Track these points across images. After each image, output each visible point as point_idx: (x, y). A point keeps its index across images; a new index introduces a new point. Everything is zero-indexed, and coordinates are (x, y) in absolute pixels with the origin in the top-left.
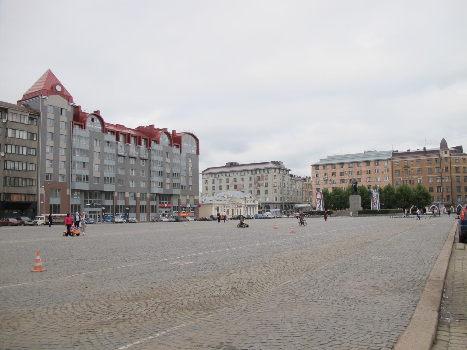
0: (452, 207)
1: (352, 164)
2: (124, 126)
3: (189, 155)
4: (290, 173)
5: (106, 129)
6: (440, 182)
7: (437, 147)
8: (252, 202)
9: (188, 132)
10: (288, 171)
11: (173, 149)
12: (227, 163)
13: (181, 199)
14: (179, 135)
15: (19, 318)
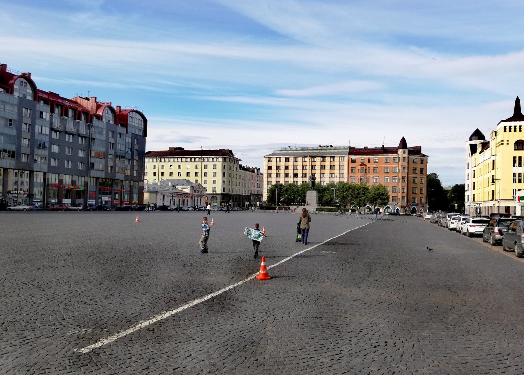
0: (407, 208)
2: (59, 95)
3: (134, 136)
4: (240, 163)
5: (39, 96)
6: (395, 182)
8: (200, 192)
9: (135, 109)
10: (238, 160)
11: (118, 128)
12: (170, 148)
13: (124, 185)
14: (124, 113)
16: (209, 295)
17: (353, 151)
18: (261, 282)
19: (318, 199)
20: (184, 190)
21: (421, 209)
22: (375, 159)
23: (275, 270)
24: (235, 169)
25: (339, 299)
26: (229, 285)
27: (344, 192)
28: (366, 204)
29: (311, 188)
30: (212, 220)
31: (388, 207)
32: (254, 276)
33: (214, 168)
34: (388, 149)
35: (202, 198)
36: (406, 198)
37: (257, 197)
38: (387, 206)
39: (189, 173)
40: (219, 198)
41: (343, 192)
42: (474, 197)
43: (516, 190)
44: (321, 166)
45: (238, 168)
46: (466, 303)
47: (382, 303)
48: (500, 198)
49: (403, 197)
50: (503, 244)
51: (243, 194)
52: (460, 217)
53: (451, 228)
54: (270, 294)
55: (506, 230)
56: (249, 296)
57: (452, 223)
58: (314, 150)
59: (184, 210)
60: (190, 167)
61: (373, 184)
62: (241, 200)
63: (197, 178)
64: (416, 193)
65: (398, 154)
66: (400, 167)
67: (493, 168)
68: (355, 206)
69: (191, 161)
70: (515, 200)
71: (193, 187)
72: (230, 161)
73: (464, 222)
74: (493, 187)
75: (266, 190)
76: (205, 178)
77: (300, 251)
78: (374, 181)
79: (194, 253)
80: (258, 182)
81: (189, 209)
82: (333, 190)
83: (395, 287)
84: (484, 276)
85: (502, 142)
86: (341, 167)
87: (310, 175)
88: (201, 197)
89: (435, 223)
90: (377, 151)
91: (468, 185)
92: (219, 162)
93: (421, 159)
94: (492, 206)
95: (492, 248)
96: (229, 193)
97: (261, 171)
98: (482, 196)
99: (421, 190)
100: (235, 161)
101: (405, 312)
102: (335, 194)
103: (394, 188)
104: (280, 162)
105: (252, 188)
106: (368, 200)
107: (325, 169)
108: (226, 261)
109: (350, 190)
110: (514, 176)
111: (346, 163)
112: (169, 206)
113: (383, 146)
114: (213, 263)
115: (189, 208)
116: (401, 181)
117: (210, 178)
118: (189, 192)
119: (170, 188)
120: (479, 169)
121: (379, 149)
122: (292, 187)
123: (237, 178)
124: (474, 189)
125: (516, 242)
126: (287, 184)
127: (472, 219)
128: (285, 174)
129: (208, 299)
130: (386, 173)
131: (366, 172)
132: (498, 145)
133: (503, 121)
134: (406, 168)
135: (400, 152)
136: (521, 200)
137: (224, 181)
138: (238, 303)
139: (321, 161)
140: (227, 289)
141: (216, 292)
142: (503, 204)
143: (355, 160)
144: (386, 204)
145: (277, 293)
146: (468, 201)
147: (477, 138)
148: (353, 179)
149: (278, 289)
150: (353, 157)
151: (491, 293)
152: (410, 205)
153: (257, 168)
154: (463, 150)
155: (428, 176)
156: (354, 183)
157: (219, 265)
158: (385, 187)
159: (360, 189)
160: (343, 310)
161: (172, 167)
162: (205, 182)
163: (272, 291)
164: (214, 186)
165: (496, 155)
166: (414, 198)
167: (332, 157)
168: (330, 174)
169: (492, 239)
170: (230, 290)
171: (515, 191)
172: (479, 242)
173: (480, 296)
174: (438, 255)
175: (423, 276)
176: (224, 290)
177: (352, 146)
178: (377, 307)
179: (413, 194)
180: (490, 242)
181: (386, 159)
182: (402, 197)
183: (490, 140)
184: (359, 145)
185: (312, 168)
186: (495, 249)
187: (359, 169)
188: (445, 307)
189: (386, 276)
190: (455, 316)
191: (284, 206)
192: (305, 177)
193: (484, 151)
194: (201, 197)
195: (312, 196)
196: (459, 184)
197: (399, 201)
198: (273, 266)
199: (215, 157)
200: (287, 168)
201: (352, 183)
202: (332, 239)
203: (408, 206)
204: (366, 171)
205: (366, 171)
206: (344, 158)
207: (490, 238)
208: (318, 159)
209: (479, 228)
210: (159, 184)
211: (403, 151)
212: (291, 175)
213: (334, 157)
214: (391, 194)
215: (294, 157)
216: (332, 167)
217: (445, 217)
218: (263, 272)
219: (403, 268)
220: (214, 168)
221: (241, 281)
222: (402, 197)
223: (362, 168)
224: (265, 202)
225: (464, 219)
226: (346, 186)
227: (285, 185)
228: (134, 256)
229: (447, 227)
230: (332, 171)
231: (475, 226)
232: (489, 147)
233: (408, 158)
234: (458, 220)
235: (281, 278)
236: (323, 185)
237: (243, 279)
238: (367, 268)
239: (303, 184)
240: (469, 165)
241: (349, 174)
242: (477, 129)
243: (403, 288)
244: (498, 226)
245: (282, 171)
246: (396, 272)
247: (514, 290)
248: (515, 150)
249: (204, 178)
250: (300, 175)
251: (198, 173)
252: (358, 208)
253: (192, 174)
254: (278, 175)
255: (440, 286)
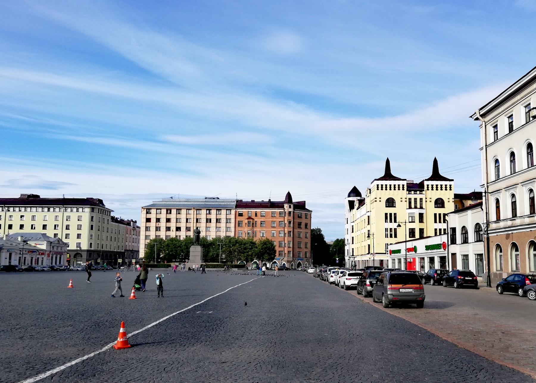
0: (292, 262)
1: (191, 210)
4: (112, 214)
6: (282, 237)
7: (282, 199)
8: (59, 248)
10: (110, 211)
12: (22, 195)
13: (115, 241)
15: (453, 319)
16: (48, 372)
17: (240, 204)
18: (118, 351)
19: (202, 255)
20: (38, 246)
21: (306, 264)
22: (262, 212)
23: (139, 336)
24: (106, 221)
25: (205, 363)
26: (77, 358)
27: (231, 247)
28: (254, 260)
29: (195, 242)
30: (71, 282)
31: (275, 262)
32: (111, 344)
33: (78, 220)
34: (275, 203)
35: (62, 256)
36: (292, 252)
37: (132, 253)
38: (274, 261)
39: (46, 225)
40: (85, 255)
41: (230, 247)
42: (353, 251)
43: (388, 244)
44: (207, 219)
45: (110, 220)
46: (332, 355)
47: (250, 362)
48: (375, 252)
49: (289, 252)
50: (373, 295)
51: (116, 251)
52: (339, 270)
53: (331, 281)
54: (126, 365)
55: (375, 282)
56: (100, 369)
57: (332, 276)
58: (196, 202)
59: (38, 271)
60: (47, 218)
61: (260, 238)
62: (113, 257)
63: (56, 232)
64: (301, 248)
65: (284, 209)
66: (286, 222)
67: (369, 224)
68: (242, 262)
69: (49, 210)
70: (388, 254)
71: (51, 243)
72: (100, 212)
73: (342, 275)
74: (369, 242)
75: (144, 245)
76: (68, 232)
77: (172, 313)
78: (261, 236)
79: (38, 322)
80: (134, 236)
81: (45, 269)
82: (219, 245)
83: (267, 345)
84: (352, 327)
85: (376, 200)
86: (228, 221)
87: (195, 228)
88: (61, 254)
89: (318, 277)
90: (264, 205)
91: (348, 239)
92: (86, 213)
93: (305, 214)
94: (368, 259)
95: (364, 300)
96: (97, 249)
97: (138, 224)
98: (359, 252)
99: (306, 244)
100: (105, 212)
101: (272, 371)
102: (221, 249)
103: (281, 242)
104: (160, 213)
105: (127, 243)
106: (255, 256)
107: (210, 222)
108: (79, 330)
109: (237, 244)
110: (386, 231)
111: (232, 217)
112: (17, 266)
113: (270, 200)
114: (60, 333)
115: (44, 267)
116: (287, 235)
117: (73, 232)
118: (45, 249)
119: (19, 244)
120: (357, 225)
121: (266, 203)
122: (174, 241)
123: (108, 232)
124: (353, 243)
125: (383, 293)
126: (168, 238)
127: (348, 273)
128: (166, 227)
129: (45, 377)
130: (273, 227)
131: (253, 226)
132: (372, 202)
133: (376, 180)
134: (292, 223)
135: (286, 206)
136: (392, 254)
137: (91, 236)
138: (84, 379)
139: (207, 214)
140: (73, 363)
141: (58, 368)
142: (378, 258)
143: (242, 213)
144: (273, 259)
145: (135, 363)
146: (348, 255)
147: (355, 195)
148: (240, 233)
149: (138, 359)
150: (240, 210)
151: (355, 344)
152: (296, 259)
153: (134, 220)
154: (343, 206)
155: (313, 231)
156: (241, 238)
157: (68, 336)
158: (272, 241)
159: (247, 244)
160: (207, 375)
161: (24, 218)
162: (67, 236)
163: (129, 361)
164: (79, 241)
165: (371, 211)
166: (299, 253)
167: (219, 210)
168: (216, 227)
169: (365, 291)
170: (77, 364)
171: (387, 245)
172: (353, 294)
173: (345, 348)
174: (314, 309)
175: (296, 332)
176: (69, 364)
177: (239, 198)
178: (244, 368)
179: (299, 249)
180: (363, 294)
181: (272, 213)
182: (288, 251)
183: (365, 197)
184: (247, 198)
185: (197, 222)
186: (366, 301)
187: (246, 223)
188: (312, 361)
189: (260, 333)
190: (319, 370)
191: (165, 263)
192: (189, 230)
193: (360, 207)
194: (61, 254)
195: (196, 251)
196: (340, 239)
197: (286, 255)
198: (137, 332)
199: (81, 207)
200: (168, 220)
201: (238, 237)
202: (211, 297)
203: (293, 260)
204: (254, 225)
205: (254, 225)
206: (230, 211)
207: (363, 290)
208: (204, 212)
209: (354, 281)
210: (4, 239)
211: (288, 205)
212: (173, 228)
213: (181, 209)
214: (277, 249)
215: (177, 209)
216: (218, 221)
217: (326, 271)
218: (122, 340)
219: (279, 324)
220: (78, 220)
221: (93, 352)
222: (288, 251)
223: (249, 222)
224: (142, 259)
225: (342, 273)
226: (232, 241)
227: (166, 239)
228: (256, 336)
229: (328, 281)
230: (218, 225)
231: (350, 279)
232: (365, 204)
233: (294, 212)
234: (336, 274)
235: (144, 345)
236: (208, 239)
237: (97, 350)
238: (243, 326)
239: (186, 238)
240: (348, 220)
241: (236, 228)
242: (355, 187)
243: (275, 346)
244: (369, 278)
245: (163, 224)
246: (271, 329)
247: (377, 340)
248: (386, 207)
249: (66, 232)
250: (183, 229)
251: (58, 225)
252: (246, 263)
253: (50, 227)
254: (158, 229)
255: (311, 341)
